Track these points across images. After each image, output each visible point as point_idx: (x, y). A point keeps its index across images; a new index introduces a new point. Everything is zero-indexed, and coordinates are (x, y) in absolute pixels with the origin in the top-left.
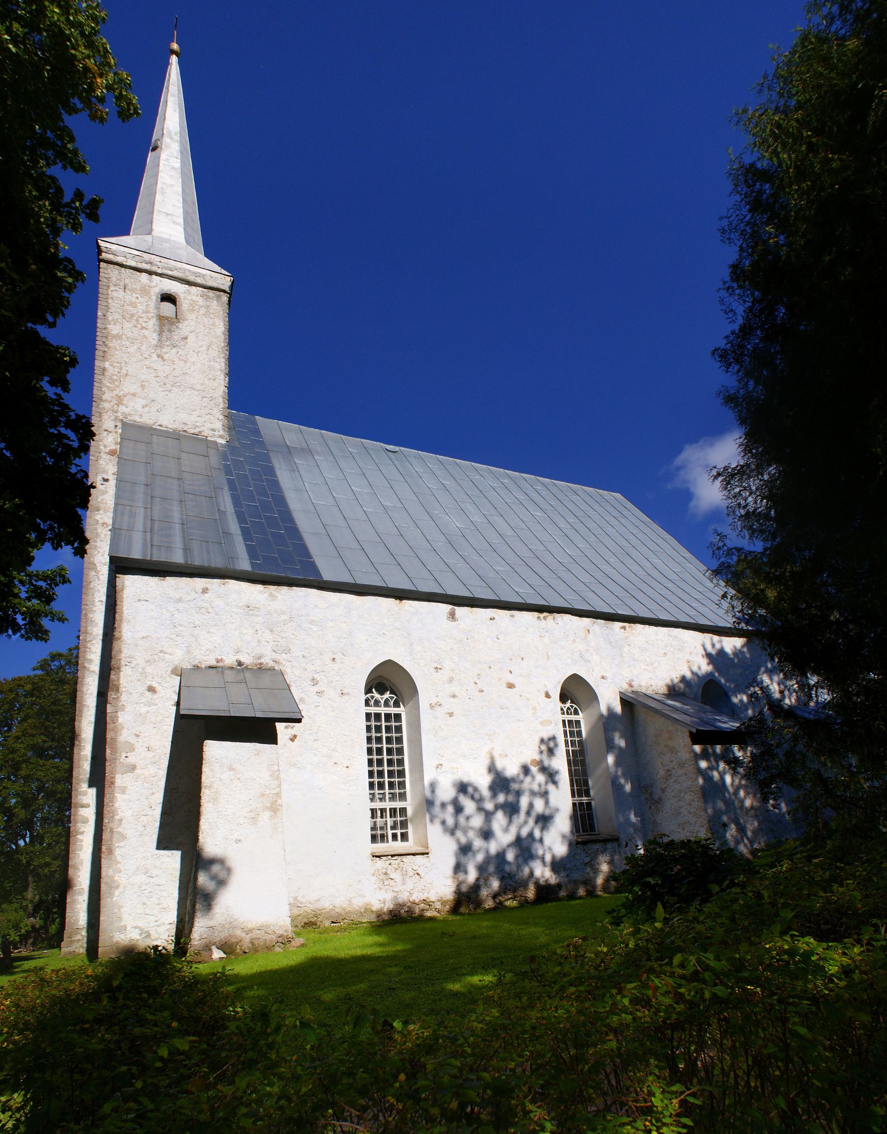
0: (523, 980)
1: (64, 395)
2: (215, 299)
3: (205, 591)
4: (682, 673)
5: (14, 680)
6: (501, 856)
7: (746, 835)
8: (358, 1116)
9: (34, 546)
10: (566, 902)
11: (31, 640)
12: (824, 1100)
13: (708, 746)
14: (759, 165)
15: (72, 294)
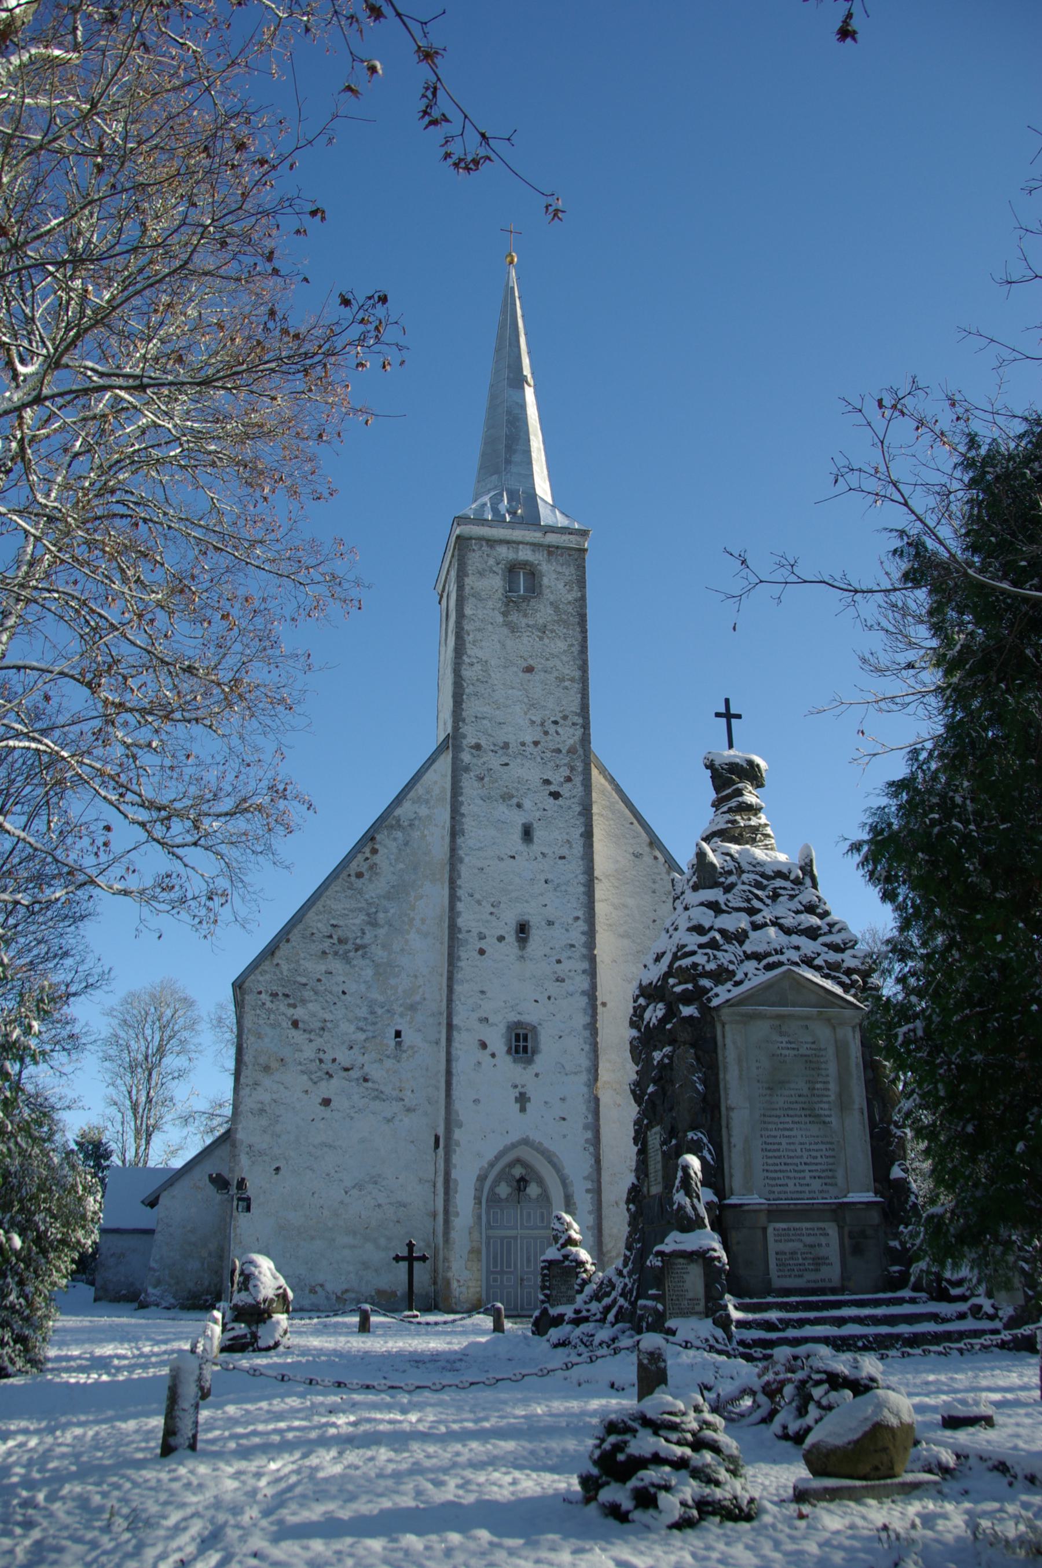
0: (577, 1312)
6: (941, 1217)
8: (945, 655)
10: (706, 1354)
13: (434, 1537)
14: (454, 1285)
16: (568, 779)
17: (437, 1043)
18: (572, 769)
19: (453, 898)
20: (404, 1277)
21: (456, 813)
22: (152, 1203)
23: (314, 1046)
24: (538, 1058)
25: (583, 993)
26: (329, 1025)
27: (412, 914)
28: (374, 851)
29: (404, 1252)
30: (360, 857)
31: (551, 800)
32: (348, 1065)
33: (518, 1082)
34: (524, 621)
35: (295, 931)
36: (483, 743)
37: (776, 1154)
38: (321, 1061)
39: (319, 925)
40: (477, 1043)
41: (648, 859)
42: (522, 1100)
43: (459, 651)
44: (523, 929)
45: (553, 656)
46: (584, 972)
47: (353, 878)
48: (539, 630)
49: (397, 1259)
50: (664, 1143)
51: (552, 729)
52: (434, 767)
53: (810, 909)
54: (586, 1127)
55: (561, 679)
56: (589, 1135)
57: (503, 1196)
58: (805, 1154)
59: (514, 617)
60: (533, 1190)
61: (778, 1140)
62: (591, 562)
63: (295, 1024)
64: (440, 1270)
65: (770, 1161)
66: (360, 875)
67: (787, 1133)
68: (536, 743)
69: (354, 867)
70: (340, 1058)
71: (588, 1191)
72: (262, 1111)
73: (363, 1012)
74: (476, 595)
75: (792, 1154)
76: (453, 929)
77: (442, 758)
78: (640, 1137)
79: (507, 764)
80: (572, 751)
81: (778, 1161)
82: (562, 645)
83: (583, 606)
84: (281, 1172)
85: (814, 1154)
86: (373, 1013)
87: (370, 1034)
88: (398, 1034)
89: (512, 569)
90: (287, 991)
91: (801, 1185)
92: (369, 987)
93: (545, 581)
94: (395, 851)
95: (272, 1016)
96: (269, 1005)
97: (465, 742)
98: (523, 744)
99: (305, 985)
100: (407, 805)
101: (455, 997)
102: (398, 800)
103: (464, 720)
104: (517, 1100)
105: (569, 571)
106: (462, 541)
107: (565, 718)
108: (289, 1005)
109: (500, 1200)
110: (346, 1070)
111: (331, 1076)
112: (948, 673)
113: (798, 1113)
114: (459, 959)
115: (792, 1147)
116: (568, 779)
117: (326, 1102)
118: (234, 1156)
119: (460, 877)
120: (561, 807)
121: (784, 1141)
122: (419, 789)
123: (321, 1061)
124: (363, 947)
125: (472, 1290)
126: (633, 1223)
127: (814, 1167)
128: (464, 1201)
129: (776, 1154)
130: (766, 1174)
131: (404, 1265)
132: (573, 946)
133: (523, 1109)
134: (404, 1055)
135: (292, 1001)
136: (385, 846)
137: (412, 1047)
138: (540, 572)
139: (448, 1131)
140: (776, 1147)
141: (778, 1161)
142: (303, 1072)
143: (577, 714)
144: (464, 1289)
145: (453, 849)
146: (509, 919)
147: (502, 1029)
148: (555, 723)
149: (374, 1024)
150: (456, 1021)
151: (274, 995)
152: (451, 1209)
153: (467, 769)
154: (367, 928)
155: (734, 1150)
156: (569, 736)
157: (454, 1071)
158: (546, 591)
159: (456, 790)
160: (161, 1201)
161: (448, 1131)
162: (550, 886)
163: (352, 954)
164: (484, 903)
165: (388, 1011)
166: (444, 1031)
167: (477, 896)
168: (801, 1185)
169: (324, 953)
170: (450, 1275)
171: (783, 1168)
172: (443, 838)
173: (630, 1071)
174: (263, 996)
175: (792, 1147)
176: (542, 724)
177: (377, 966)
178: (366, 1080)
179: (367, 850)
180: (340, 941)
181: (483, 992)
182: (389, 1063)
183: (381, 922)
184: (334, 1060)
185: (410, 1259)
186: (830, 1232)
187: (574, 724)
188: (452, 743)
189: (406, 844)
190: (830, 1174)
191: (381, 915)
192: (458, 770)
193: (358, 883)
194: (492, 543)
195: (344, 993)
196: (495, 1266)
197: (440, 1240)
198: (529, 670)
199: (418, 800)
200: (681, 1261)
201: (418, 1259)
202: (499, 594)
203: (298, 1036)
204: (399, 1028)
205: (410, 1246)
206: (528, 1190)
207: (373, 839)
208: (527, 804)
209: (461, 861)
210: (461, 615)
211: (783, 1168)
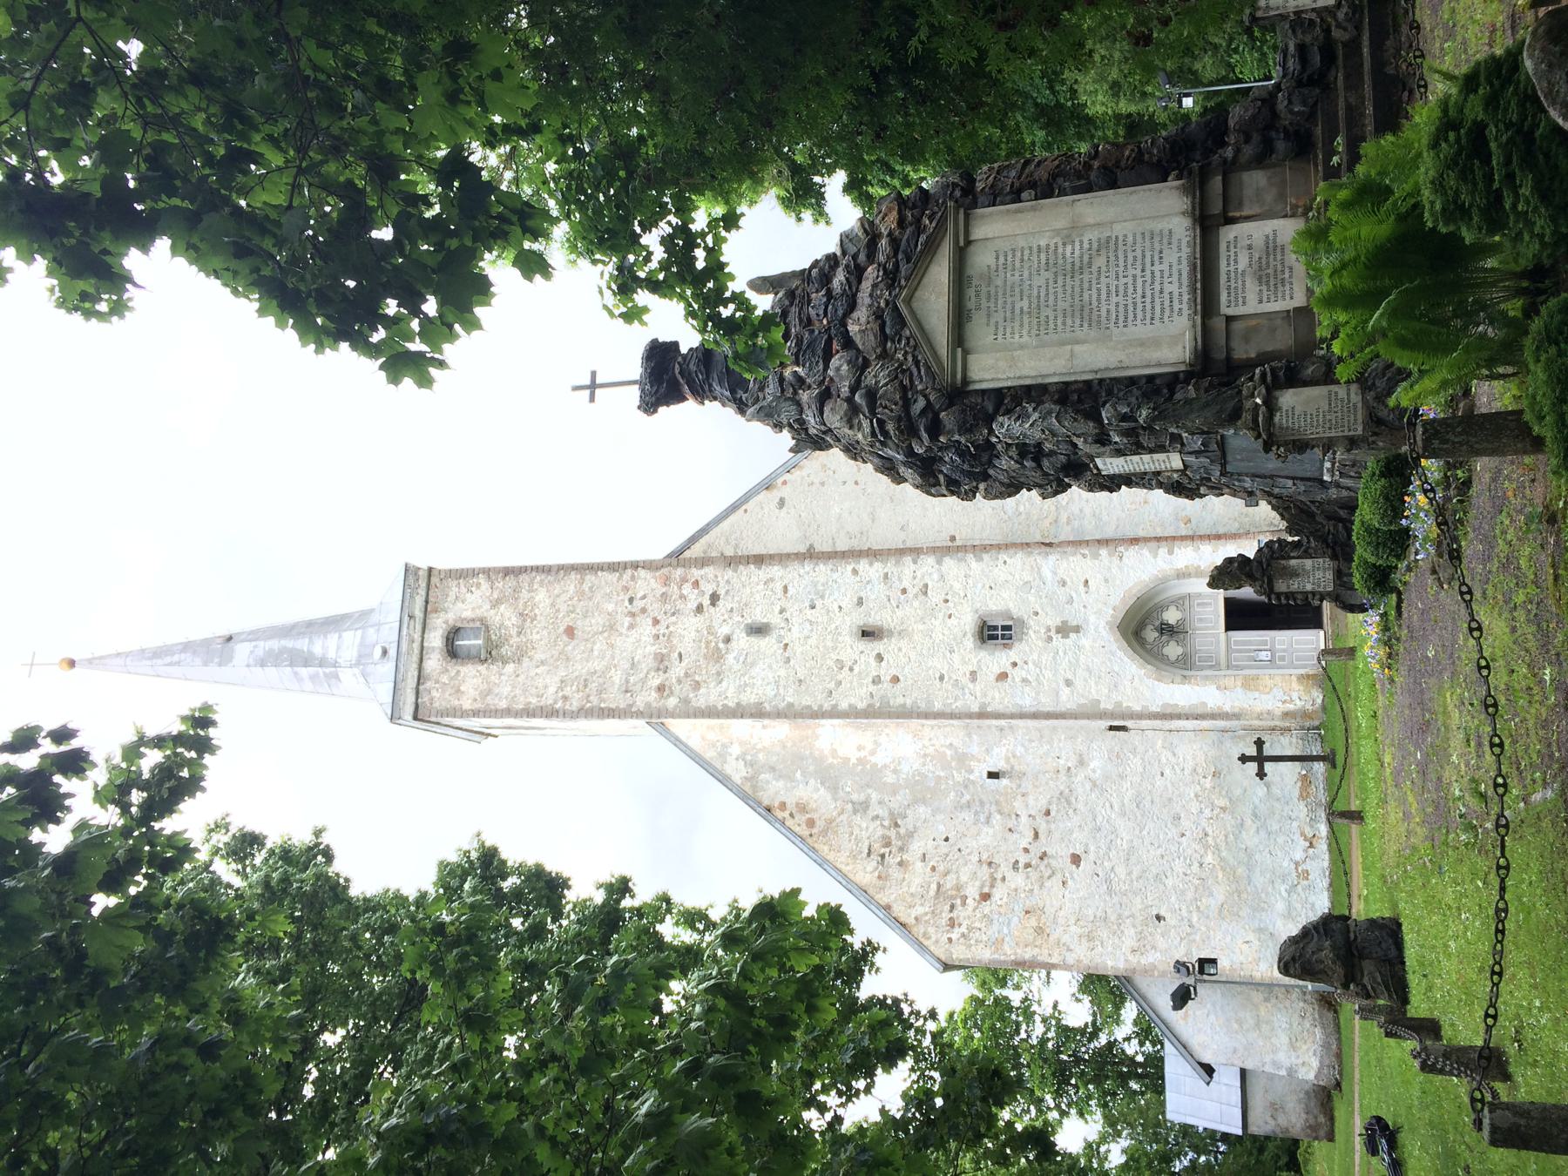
1: (269, 844)
2: (1372, 230)
3: (746, 511)
4: (779, 210)
5: (969, 495)
7: (946, 475)
9: (1472, 406)
11: (1256, 439)
12: (181, 746)
14: (1291, 707)
15: (734, 232)
16: (696, 584)
18: (684, 580)
19: (834, 713)
21: (738, 712)
22: (1209, 1070)
23: (1010, 874)
24: (1016, 613)
25: (939, 562)
26: (984, 857)
27: (854, 760)
28: (783, 806)
29: (1252, 767)
30: (789, 822)
31: (721, 603)
32: (1032, 834)
33: (1045, 636)
34: (514, 640)
35: (877, 897)
36: (657, 682)
37: (1131, 308)
38: (1028, 865)
39: (869, 869)
40: (999, 684)
41: (785, 492)
42: (1065, 630)
43: (550, 713)
44: (867, 634)
45: (553, 605)
46: (915, 562)
47: (814, 831)
48: (525, 620)
49: (1261, 774)
51: (639, 604)
52: (684, 739)
53: (825, 279)
54: (1096, 556)
55: (581, 594)
56: (1104, 552)
57: (1180, 650)
58: (1131, 271)
60: (1171, 616)
61: (1113, 308)
64: (1272, 724)
65: (1140, 315)
66: (811, 823)
67: (1104, 296)
68: (656, 622)
71: (1171, 552)
72: (1090, 938)
73: (967, 816)
75: (1131, 290)
76: (870, 713)
78: (1112, 483)
79: (680, 655)
80: (666, 581)
81: (1140, 306)
83: (497, 571)
84: (1162, 913)
86: (968, 805)
87: (993, 808)
88: (993, 775)
89: (452, 651)
90: (947, 907)
92: (935, 812)
94: (781, 784)
95: (977, 925)
96: (963, 929)
97: (654, 705)
99: (939, 884)
101: (948, 710)
102: (724, 780)
103: (631, 706)
104: (1066, 636)
105: (454, 589)
106: (415, 718)
107: (626, 589)
108: (964, 904)
109: (1185, 655)
110: (1036, 835)
111: (1045, 854)
112: (1295, 13)
113: (1077, 283)
114: (904, 705)
115: (1121, 289)
116: (696, 584)
117: (1076, 860)
118: (1147, 971)
119: (809, 707)
121: (1114, 299)
122: (709, 755)
123: (1028, 865)
124: (891, 814)
125: (1295, 685)
126: (1218, 490)
127: (1148, 260)
129: (1131, 308)
130: (1156, 321)
131: (1269, 767)
132: (886, 575)
133: (1077, 629)
134: (1017, 768)
135: (958, 902)
136: (777, 793)
137: (1007, 760)
139: (1102, 715)
141: (1140, 306)
142: (1042, 886)
143: (621, 575)
144: (1295, 696)
145: (779, 714)
147: (983, 654)
148: (631, 600)
149: (982, 803)
150: (975, 708)
151: (952, 923)
152: (1199, 711)
153: (686, 701)
154: (871, 813)
155: (1127, 363)
157: (1033, 710)
158: (479, 613)
159: (710, 713)
160: (1205, 1060)
161: (1102, 715)
162: (818, 603)
163: (902, 831)
164: (840, 677)
165: (966, 787)
166: (988, 722)
167: (832, 685)
169: (901, 864)
170: (1278, 712)
171: (1148, 300)
172: (764, 727)
173: (1028, 499)
174: (954, 936)
175: (1121, 289)
176: (633, 615)
177: (916, 801)
178: (1048, 813)
180: (888, 844)
181: (942, 678)
182: (1027, 785)
184: (1026, 850)
185: (1261, 759)
186: (1231, 236)
187: (633, 578)
188: (655, 717)
189: (773, 769)
190: (1157, 239)
191: (855, 797)
193: (820, 824)
195: (947, 839)
198: (570, 632)
199: (723, 756)
200: (1277, 419)
201: (1251, 759)
202: (482, 668)
203: (999, 894)
204: (985, 775)
205: (1244, 759)
206: (1172, 621)
208: (724, 630)
209: (791, 705)
210: (508, 712)
211: (1148, 300)
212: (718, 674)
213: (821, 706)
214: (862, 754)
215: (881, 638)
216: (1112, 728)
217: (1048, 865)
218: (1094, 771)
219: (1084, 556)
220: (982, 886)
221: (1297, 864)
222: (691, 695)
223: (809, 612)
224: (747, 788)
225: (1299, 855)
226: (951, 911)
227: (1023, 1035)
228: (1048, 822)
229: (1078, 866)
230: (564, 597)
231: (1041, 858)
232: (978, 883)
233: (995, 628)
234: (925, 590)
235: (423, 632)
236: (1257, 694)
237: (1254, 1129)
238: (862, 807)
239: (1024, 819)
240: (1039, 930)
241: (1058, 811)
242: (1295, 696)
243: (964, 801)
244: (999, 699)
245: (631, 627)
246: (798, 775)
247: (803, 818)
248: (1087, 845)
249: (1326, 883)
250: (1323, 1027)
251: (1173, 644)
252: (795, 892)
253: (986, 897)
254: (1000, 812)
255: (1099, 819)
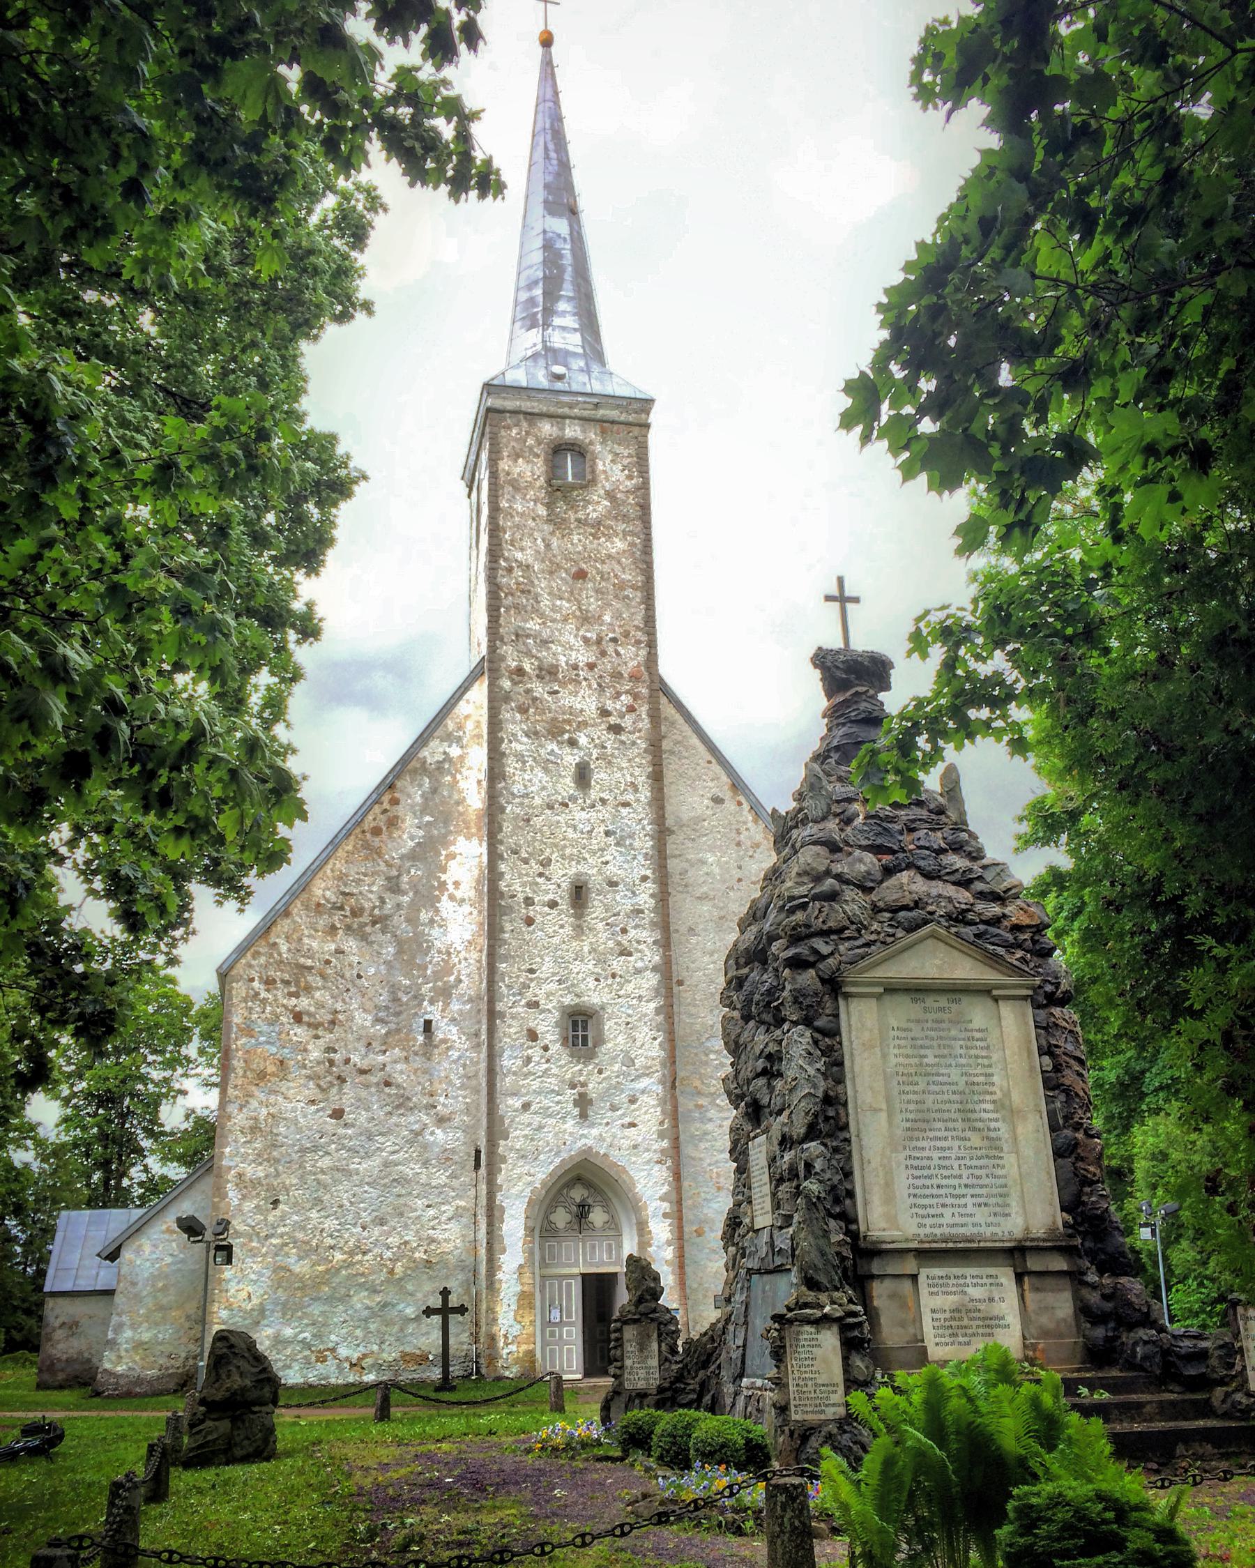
16: (631, 709)
17: (477, 1035)
18: (636, 696)
20: (437, 1335)
21: (496, 756)
26: (341, 1017)
27: (443, 877)
28: (395, 802)
29: (437, 1302)
30: (377, 809)
34: (572, 516)
38: (332, 1063)
39: (328, 893)
41: (730, 805)
42: (583, 1103)
43: (494, 553)
44: (579, 893)
47: (368, 836)
50: (772, 1160)
54: (661, 1135)
57: (561, 1225)
58: (965, 1173)
59: (561, 506)
61: (926, 1154)
62: (656, 440)
63: (298, 1017)
67: (939, 1144)
68: (591, 666)
69: (369, 823)
70: (355, 1058)
71: (665, 1215)
72: (255, 1129)
73: (384, 999)
74: (515, 485)
75: (945, 1173)
77: (476, 686)
78: (739, 1152)
80: (634, 677)
81: (928, 1182)
82: (619, 545)
85: (977, 1172)
86: (396, 1000)
87: (393, 1026)
89: (559, 449)
90: (286, 977)
91: (961, 1215)
93: (600, 466)
94: (418, 799)
96: (263, 994)
98: (575, 667)
100: (434, 744)
102: (422, 740)
103: (502, 640)
104: (576, 1103)
107: (626, 634)
108: (291, 995)
109: (556, 1230)
110: (363, 1072)
114: (502, 931)
115: (947, 1163)
116: (631, 709)
118: (220, 1192)
120: (623, 742)
121: (936, 1155)
125: (524, 1348)
127: (978, 1191)
128: (514, 1226)
129: (925, 1173)
132: (642, 912)
134: (436, 1051)
135: (293, 989)
136: (409, 796)
137: (445, 1041)
138: (593, 452)
140: (925, 1162)
141: (928, 1182)
142: (309, 1078)
144: (513, 1348)
146: (563, 874)
149: (398, 1014)
150: (500, 1007)
151: (269, 983)
152: (497, 1246)
153: (507, 698)
154: (387, 896)
156: (632, 657)
161: (492, 1143)
162: (611, 840)
163: (368, 929)
164: (533, 863)
166: (485, 1021)
168: (961, 1215)
172: (479, 782)
174: (256, 984)
175: (947, 1163)
178: (388, 1084)
179: (386, 798)
182: (418, 1062)
183: (405, 886)
185: (445, 1311)
186: (1003, 1280)
188: (490, 667)
189: (434, 791)
191: (405, 878)
192: (496, 701)
194: (532, 416)
195: (359, 976)
196: (552, 1351)
197: (483, 1283)
199: (449, 738)
200: (808, 1328)
202: (542, 481)
203: (300, 1033)
205: (445, 1293)
207: (391, 787)
208: (583, 740)
211: (935, 1191)
212: (536, 733)
213: (501, 842)
214: (451, 887)
215: (573, 907)
216: (478, 1152)
217: (331, 1085)
218: (432, 1133)
219: (662, 1123)
220: (309, 1014)
221: (333, 1350)
222: (590, 585)
223: (602, 829)
224: (414, 764)
225: (343, 1352)
226: (283, 981)
227: (151, 1058)
228: (378, 1084)
229: (331, 1116)
230: (617, 568)
231: (339, 1077)
232: (312, 1009)
233: (585, 1028)
234: (625, 953)
235: (581, 419)
236: (514, 1307)
237: (50, 1303)
238: (394, 886)
239: (381, 1058)
240: (262, 1075)
241: (389, 1095)
242: (513, 1348)
243: (400, 994)
244: (510, 1031)
245: (586, 640)
246: (428, 818)
247: (382, 822)
248: (353, 1126)
249: (312, 1380)
250: (159, 1378)
251: (568, 1217)
252: (304, 816)
253: (298, 1017)
254: (388, 1033)
255: (381, 1139)
